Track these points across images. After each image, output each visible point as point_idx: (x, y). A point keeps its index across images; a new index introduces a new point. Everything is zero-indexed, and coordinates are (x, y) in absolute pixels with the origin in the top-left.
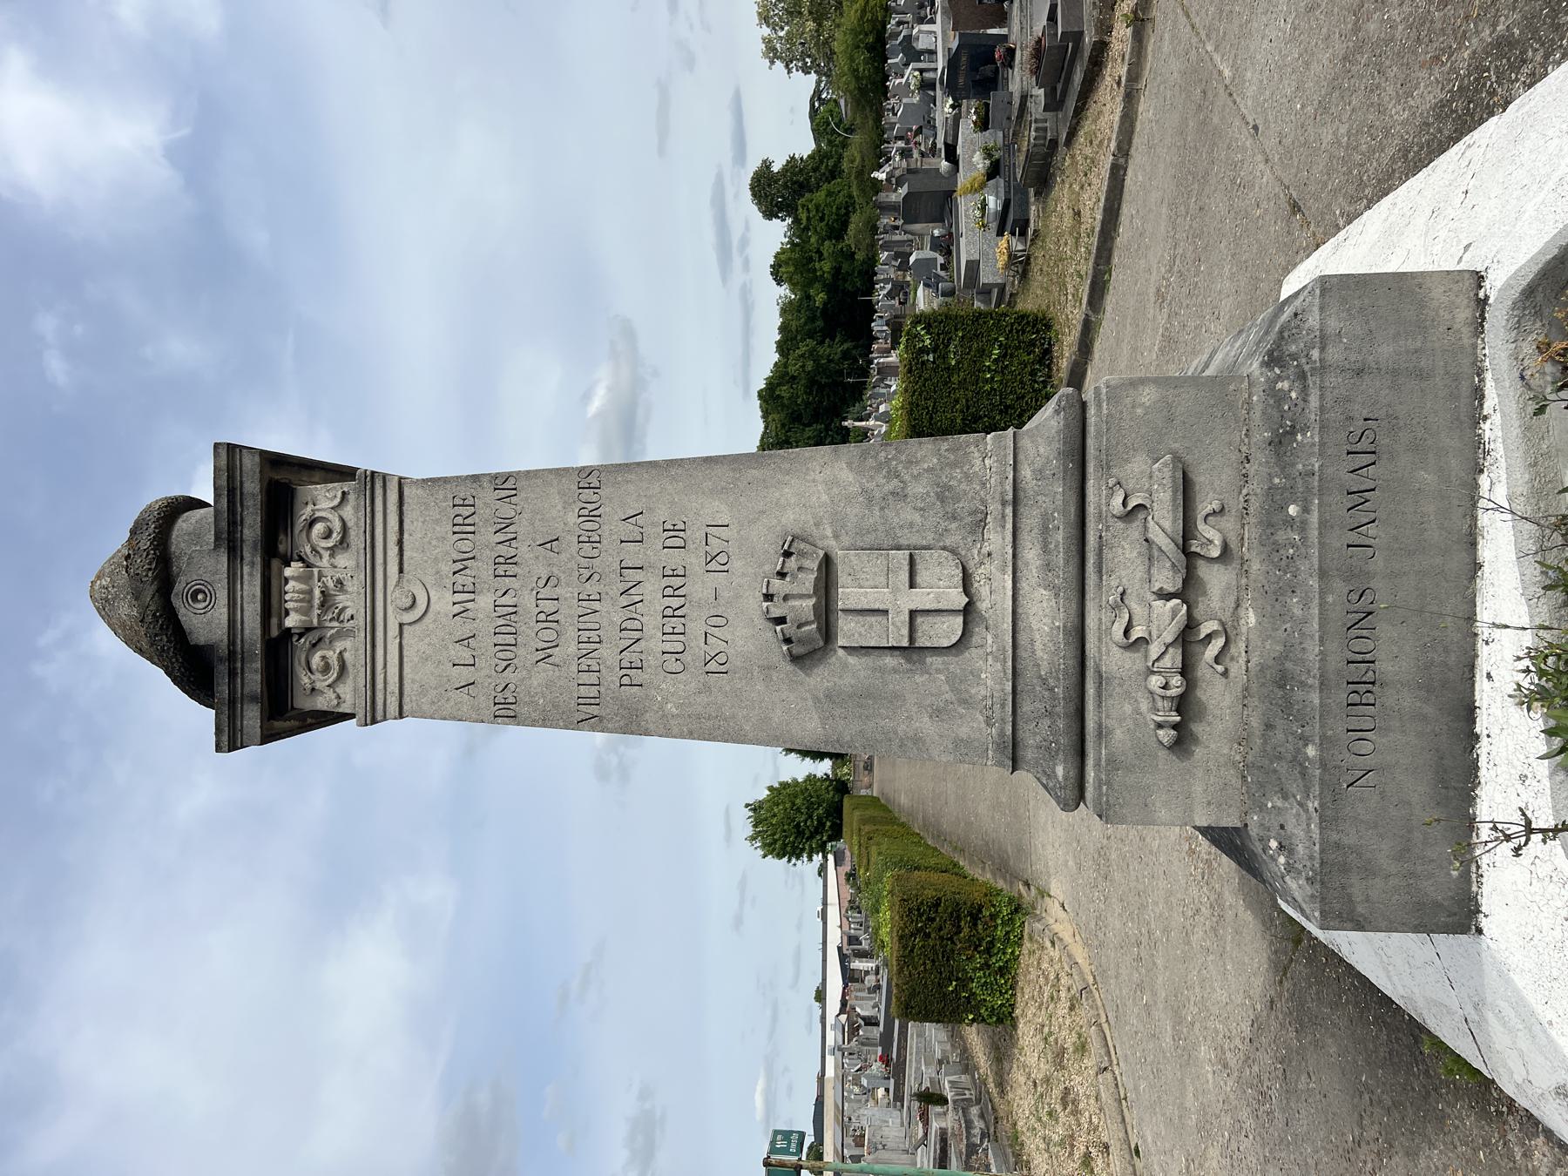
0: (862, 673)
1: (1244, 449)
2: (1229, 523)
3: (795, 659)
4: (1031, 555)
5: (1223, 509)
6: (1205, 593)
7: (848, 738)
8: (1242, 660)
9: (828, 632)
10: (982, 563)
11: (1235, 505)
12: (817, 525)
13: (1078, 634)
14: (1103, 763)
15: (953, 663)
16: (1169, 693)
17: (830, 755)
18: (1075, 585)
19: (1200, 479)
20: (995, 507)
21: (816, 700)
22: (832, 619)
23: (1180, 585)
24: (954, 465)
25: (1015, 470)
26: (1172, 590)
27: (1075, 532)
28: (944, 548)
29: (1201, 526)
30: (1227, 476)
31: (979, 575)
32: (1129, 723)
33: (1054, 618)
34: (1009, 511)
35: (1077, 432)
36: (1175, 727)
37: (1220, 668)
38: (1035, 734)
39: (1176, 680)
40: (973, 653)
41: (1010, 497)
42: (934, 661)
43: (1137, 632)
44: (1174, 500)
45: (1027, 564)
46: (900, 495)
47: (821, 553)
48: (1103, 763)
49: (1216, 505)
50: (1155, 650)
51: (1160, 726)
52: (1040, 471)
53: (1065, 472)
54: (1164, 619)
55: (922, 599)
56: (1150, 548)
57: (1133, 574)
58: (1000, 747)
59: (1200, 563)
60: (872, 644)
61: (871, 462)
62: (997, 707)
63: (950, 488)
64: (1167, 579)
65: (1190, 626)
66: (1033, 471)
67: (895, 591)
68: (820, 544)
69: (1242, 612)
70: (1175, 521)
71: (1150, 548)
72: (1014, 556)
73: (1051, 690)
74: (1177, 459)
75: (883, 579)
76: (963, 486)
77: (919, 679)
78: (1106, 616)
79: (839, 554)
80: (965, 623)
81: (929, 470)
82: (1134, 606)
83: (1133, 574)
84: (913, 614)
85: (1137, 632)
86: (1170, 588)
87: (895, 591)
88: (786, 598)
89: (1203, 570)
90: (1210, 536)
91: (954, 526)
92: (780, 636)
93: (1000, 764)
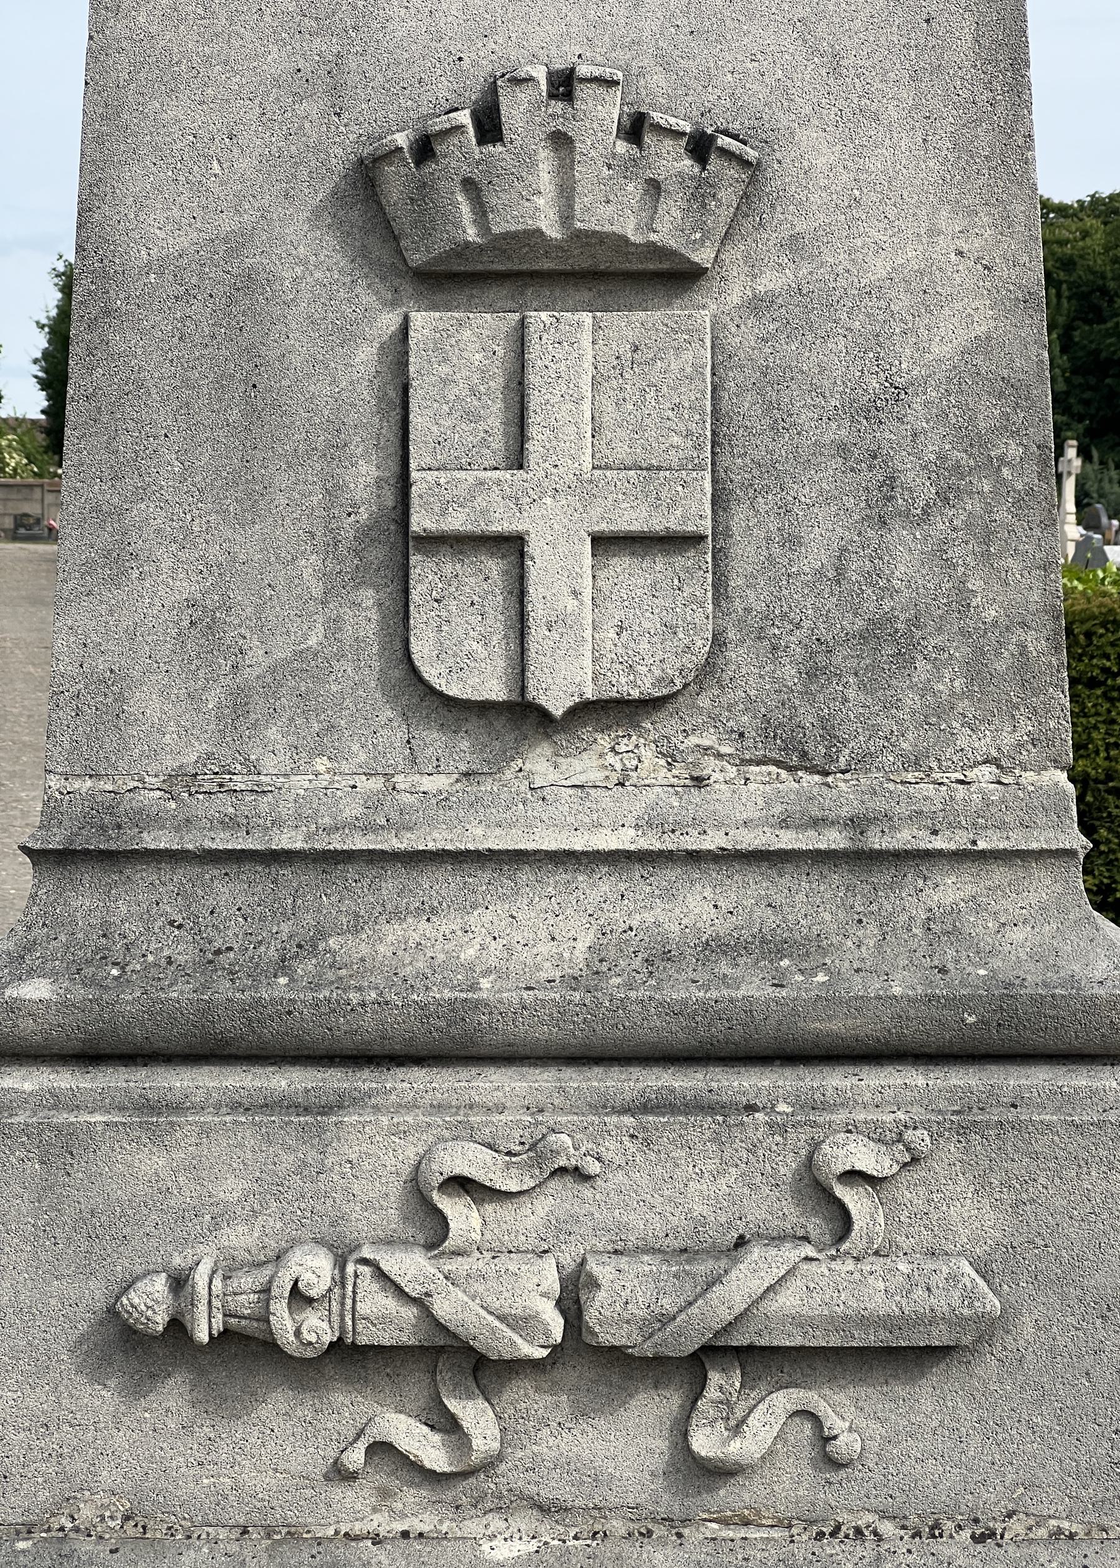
0: (321, 389)
1: (1017, 1527)
2: (793, 1484)
3: (366, 174)
4: (697, 907)
5: (836, 1464)
6: (581, 1413)
7: (117, 342)
8: (381, 1523)
9: (452, 278)
10: (671, 759)
11: (847, 1500)
12: (794, 244)
13: (456, 1045)
14: (61, 1118)
15: (360, 674)
16: (280, 1309)
17: (56, 411)
18: (605, 1034)
19: (926, 1400)
20: (845, 794)
21: (236, 244)
22: (495, 293)
23: (606, 1337)
24: (976, 670)
25: (960, 857)
26: (591, 1316)
27: (767, 1034)
28: (718, 641)
29: (783, 1401)
30: (938, 1482)
31: (640, 750)
32: (187, 1193)
33: (502, 974)
34: (834, 839)
35: (1072, 1038)
36: (177, 1327)
37: (356, 1457)
38: (147, 919)
39: (318, 1328)
40: (391, 731)
41: (877, 841)
42: (364, 614)
43: (461, 1214)
44: (864, 1321)
45: (669, 895)
46: (884, 505)
47: (703, 256)
48: (61, 1118)
49: (846, 1443)
50: (410, 1266)
51: (179, 1282)
52: (954, 932)
53: (952, 1002)
54: (502, 1291)
55: (560, 569)
56: (716, 1252)
57: (651, 1203)
58: (105, 813)
59: (672, 1401)
60: (417, 419)
61: (988, 413)
62: (225, 805)
63: (904, 659)
64: (625, 1297)
65: (484, 1370)
66: (954, 911)
67: (584, 489)
68: (734, 253)
69: (525, 1521)
70: (799, 1321)
71: (716, 1252)
72: (694, 857)
73: (283, 965)
74: (989, 1329)
75: (622, 452)
76: (911, 700)
77: (309, 566)
78: (512, 1125)
79: (701, 311)
80: (484, 708)
81: (962, 600)
82: (542, 1207)
83: (651, 1203)
84: (512, 546)
85: (461, 1214)
86: (599, 1309)
87: (584, 489)
88: (561, 141)
89: (648, 1412)
90: (755, 1428)
91: (789, 672)
92: (441, 123)
93: (52, 812)
